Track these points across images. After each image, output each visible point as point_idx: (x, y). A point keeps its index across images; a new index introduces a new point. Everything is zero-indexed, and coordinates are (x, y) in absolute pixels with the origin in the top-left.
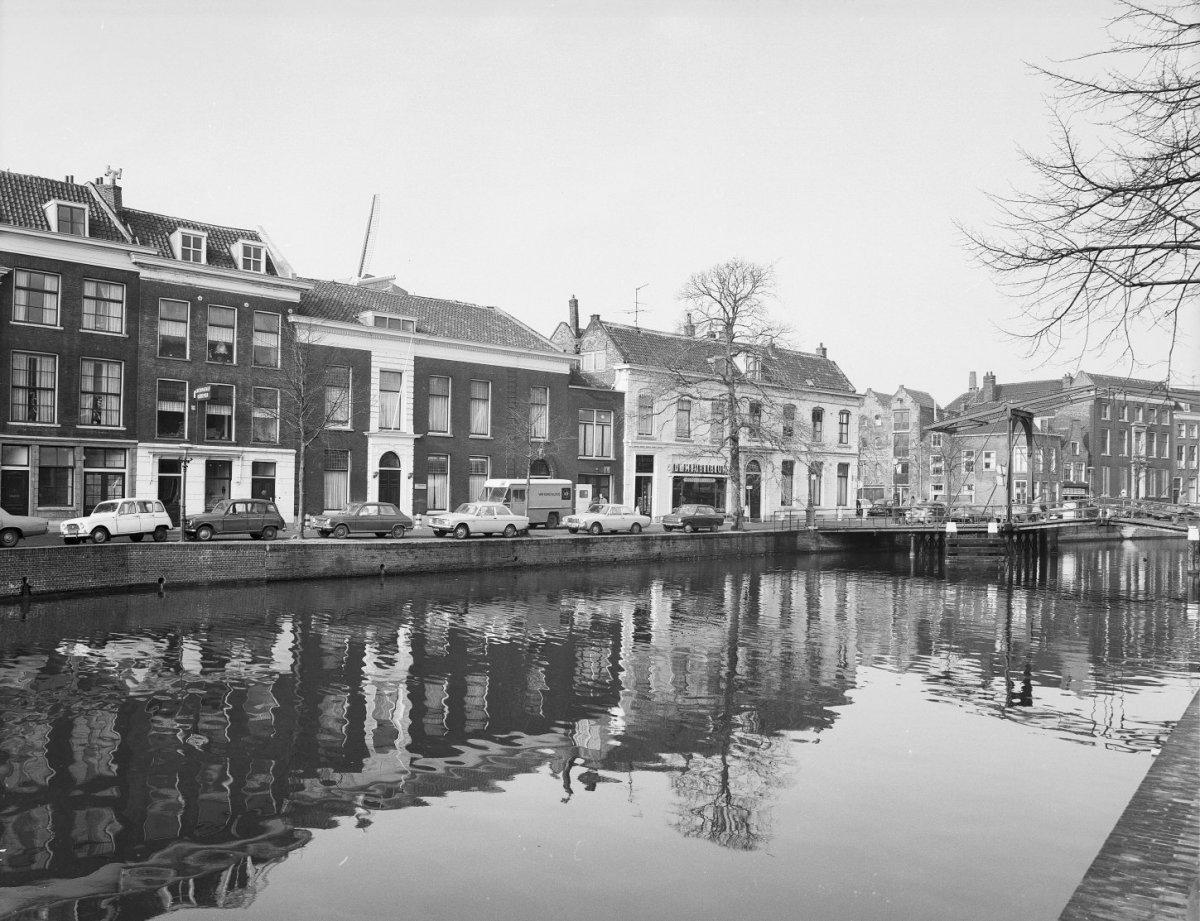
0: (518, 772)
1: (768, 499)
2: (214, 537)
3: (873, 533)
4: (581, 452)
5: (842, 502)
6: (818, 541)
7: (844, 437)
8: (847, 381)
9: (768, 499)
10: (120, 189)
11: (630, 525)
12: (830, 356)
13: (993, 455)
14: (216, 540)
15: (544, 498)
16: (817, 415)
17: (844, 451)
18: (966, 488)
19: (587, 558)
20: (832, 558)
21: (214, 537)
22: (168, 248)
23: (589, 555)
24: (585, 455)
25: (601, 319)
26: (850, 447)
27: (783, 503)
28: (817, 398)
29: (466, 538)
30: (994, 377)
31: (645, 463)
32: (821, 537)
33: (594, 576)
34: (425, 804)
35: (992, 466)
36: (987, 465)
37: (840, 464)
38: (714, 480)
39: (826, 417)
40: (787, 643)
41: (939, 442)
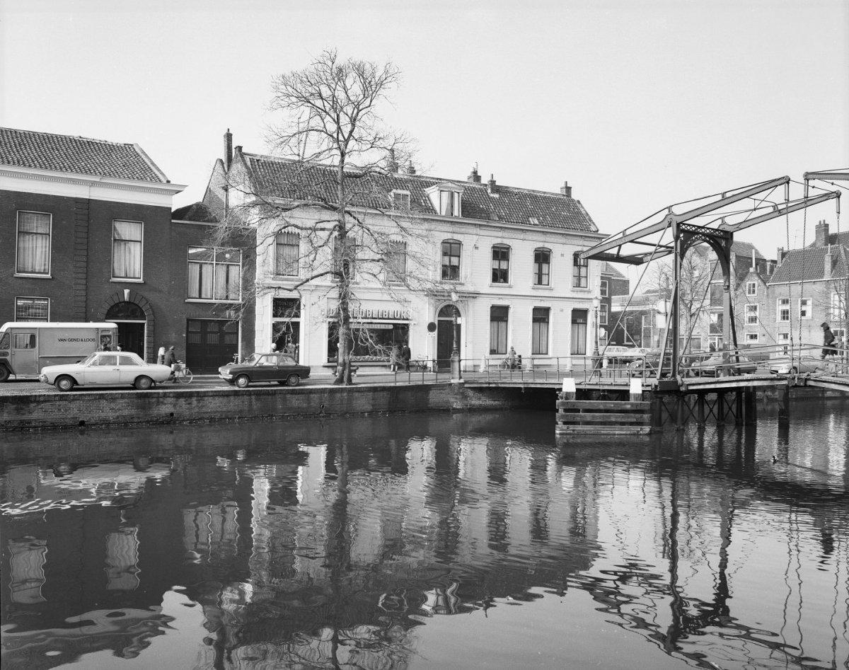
0: (533, 586)
1: (470, 346)
2: (250, 384)
3: (521, 388)
4: (194, 291)
5: (577, 352)
6: (465, 397)
7: (583, 281)
8: (590, 220)
9: (470, 346)
10: (231, 135)
11: (132, 377)
12: (575, 195)
13: (809, 303)
14: (252, 386)
15: (67, 344)
16: (542, 257)
17: (546, 293)
18: (782, 337)
19: (22, 422)
20: (489, 417)
21: (250, 384)
22: (428, 202)
23: (26, 417)
24: (200, 297)
25: (244, 150)
26: (589, 292)
27: (493, 352)
28: (541, 237)
29: (71, 389)
30: (827, 226)
31: (284, 306)
32: (471, 393)
33: (35, 445)
34: (495, 606)
35: (809, 314)
36: (803, 313)
37: (493, 307)
38: (391, 327)
39: (554, 259)
40: (498, 519)
41: (754, 292)
